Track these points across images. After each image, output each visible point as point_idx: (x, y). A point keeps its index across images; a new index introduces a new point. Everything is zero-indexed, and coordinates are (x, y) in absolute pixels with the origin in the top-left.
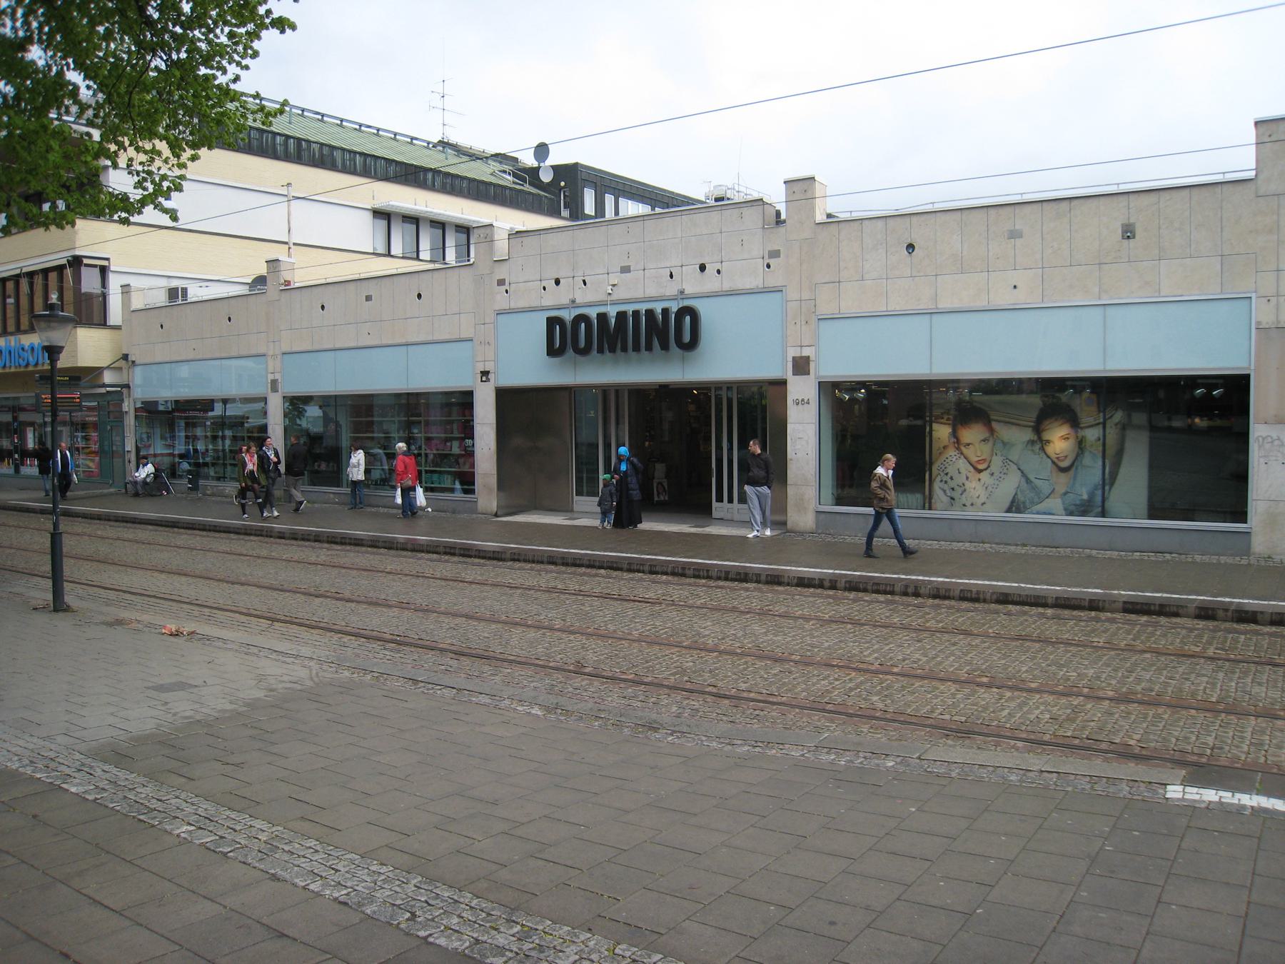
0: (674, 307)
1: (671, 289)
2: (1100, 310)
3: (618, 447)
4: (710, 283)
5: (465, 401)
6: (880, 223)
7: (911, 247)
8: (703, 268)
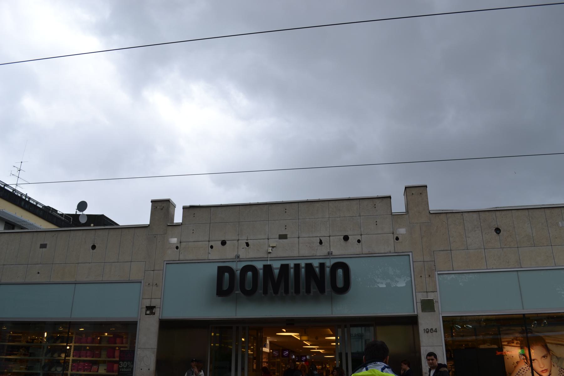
0: (329, 263)
1: (322, 251)
2: (516, 273)
3: (118, 347)
4: (352, 248)
5: (128, 329)
6: (475, 215)
7: (498, 231)
8: (346, 238)
